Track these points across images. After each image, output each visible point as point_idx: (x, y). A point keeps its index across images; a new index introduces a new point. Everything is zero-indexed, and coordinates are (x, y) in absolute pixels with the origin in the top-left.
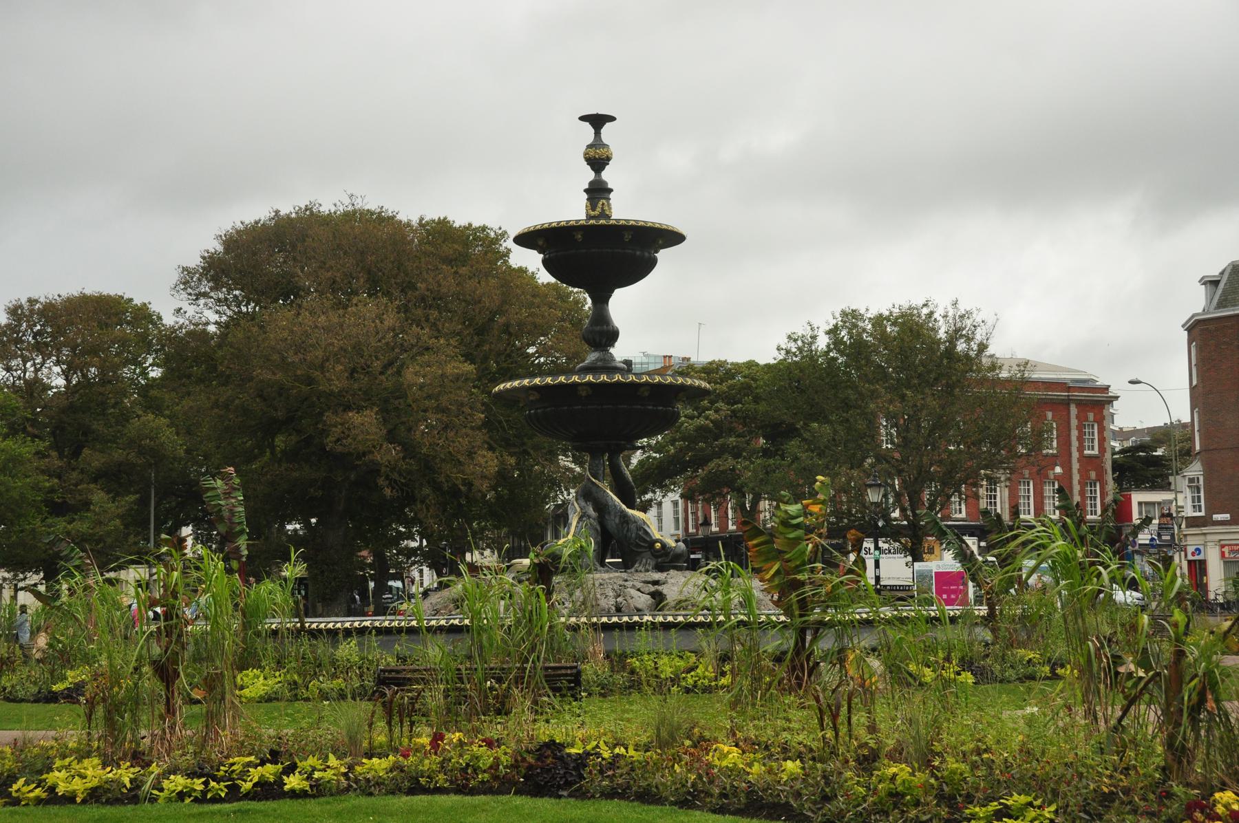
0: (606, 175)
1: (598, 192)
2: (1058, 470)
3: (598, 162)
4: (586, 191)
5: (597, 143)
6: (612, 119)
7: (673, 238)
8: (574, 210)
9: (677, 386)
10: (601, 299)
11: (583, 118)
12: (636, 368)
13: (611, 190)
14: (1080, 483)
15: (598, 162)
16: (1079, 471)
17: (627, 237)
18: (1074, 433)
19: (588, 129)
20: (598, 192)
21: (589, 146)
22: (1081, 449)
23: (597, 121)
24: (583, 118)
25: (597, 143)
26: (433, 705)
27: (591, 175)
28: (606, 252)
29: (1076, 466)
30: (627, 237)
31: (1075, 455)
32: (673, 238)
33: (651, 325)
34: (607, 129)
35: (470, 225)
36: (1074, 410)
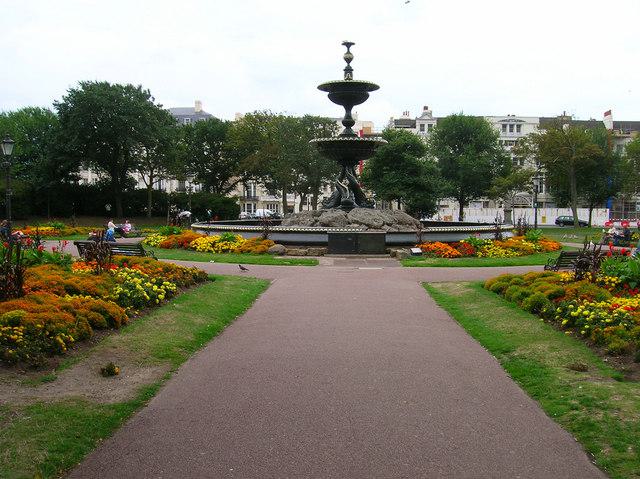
1: (348, 70)
3: (348, 60)
5: (348, 52)
7: (374, 87)
8: (340, 77)
10: (348, 109)
11: (323, 88)
12: (481, 205)
15: (348, 60)
19: (345, 48)
20: (348, 70)
23: (348, 45)
24: (323, 88)
25: (348, 52)
27: (346, 64)
28: (349, 92)
32: (374, 87)
33: (373, 117)
34: (352, 48)
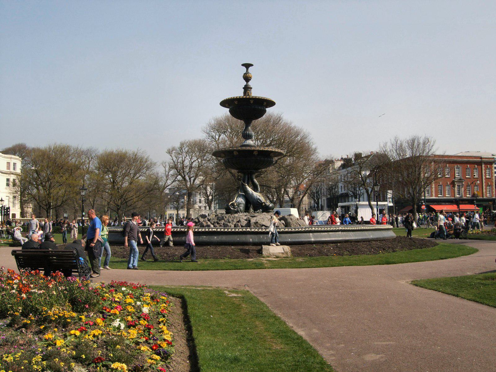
0: (250, 83)
1: (247, 89)
2: (478, 182)
4: (243, 88)
6: (252, 65)
9: (276, 152)
11: (243, 65)
13: (251, 88)
14: (485, 186)
15: (247, 78)
16: (485, 182)
17: (252, 102)
18: (483, 171)
21: (244, 74)
22: (485, 176)
23: (247, 66)
24: (243, 65)
25: (247, 72)
26: (100, 322)
27: (245, 83)
29: (484, 181)
30: (252, 102)
31: (484, 178)
34: (250, 68)
35: (291, 123)
36: (483, 165)
